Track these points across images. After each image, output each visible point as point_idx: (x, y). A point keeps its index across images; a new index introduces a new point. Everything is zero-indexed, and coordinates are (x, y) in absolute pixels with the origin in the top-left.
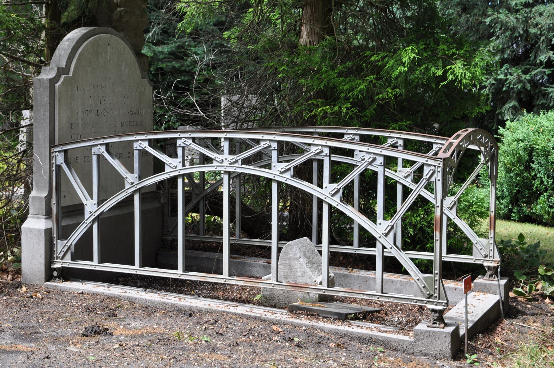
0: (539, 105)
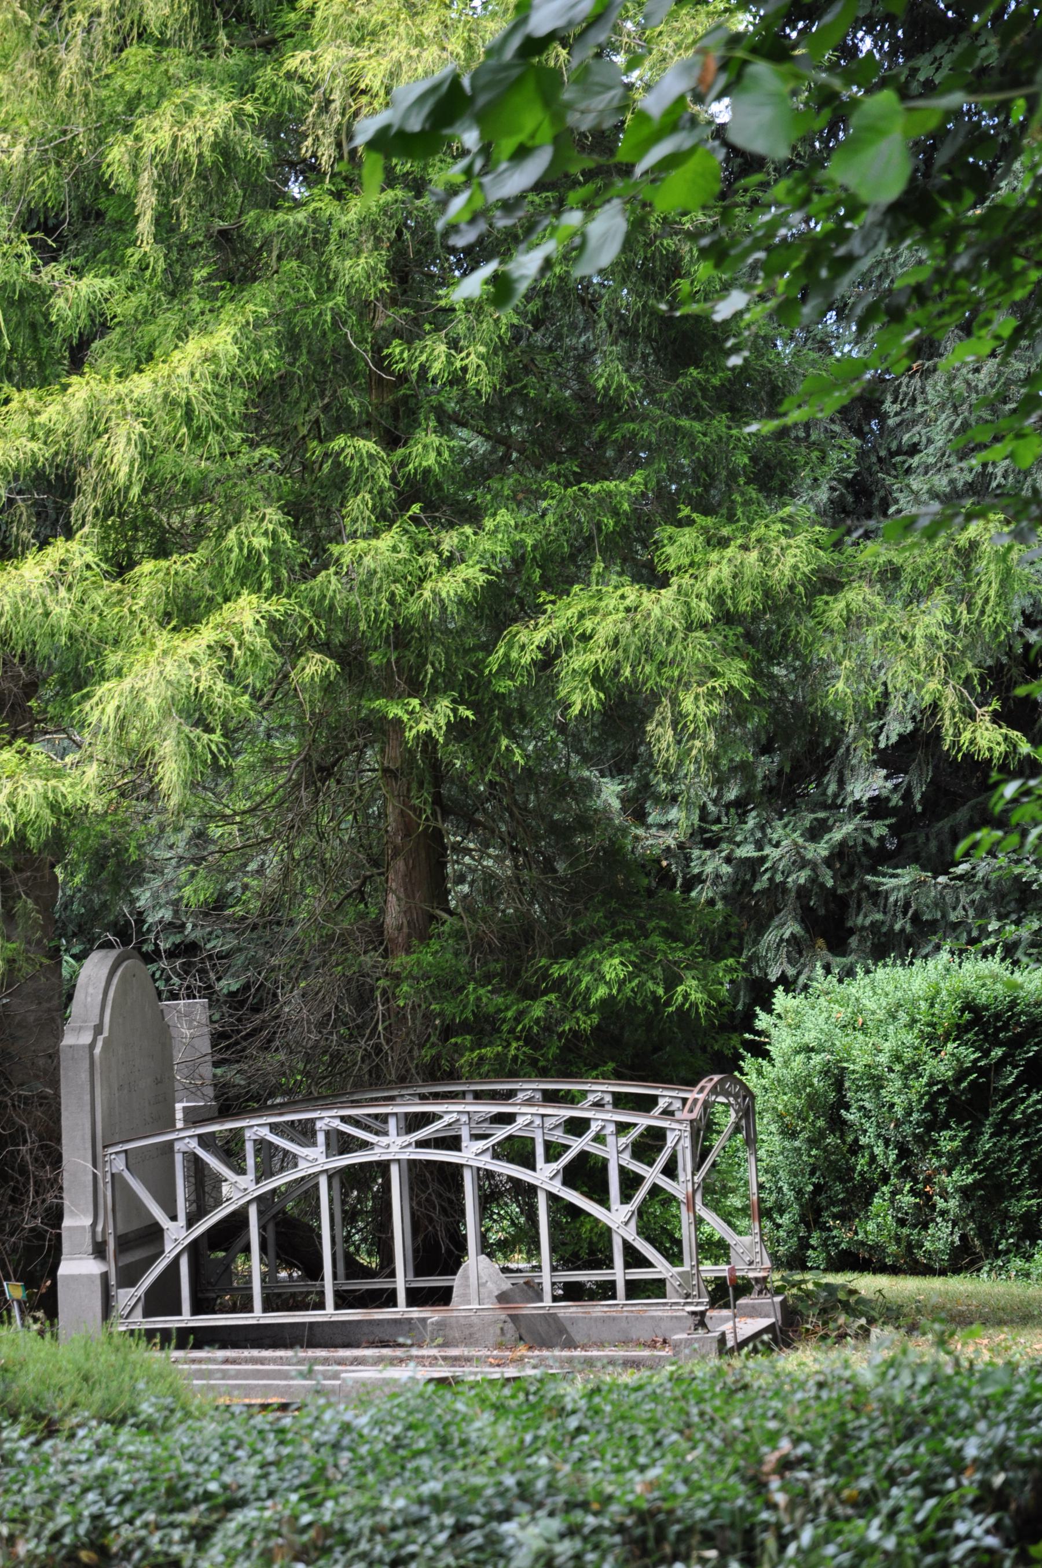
0: (863, 928)
